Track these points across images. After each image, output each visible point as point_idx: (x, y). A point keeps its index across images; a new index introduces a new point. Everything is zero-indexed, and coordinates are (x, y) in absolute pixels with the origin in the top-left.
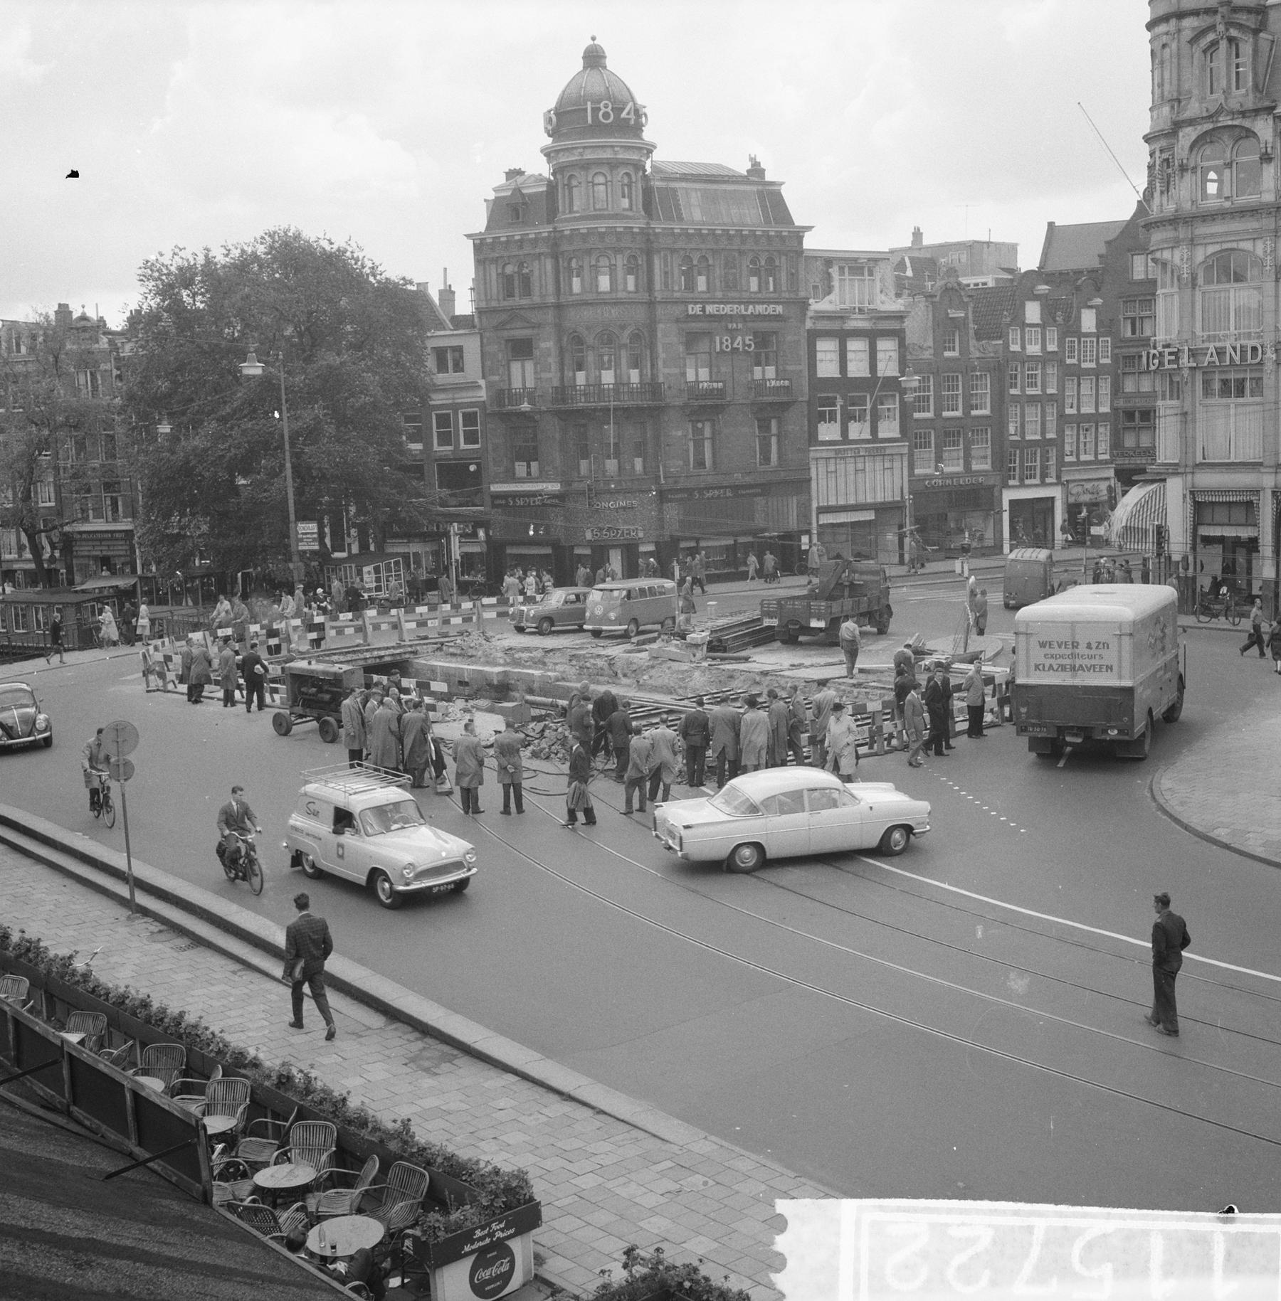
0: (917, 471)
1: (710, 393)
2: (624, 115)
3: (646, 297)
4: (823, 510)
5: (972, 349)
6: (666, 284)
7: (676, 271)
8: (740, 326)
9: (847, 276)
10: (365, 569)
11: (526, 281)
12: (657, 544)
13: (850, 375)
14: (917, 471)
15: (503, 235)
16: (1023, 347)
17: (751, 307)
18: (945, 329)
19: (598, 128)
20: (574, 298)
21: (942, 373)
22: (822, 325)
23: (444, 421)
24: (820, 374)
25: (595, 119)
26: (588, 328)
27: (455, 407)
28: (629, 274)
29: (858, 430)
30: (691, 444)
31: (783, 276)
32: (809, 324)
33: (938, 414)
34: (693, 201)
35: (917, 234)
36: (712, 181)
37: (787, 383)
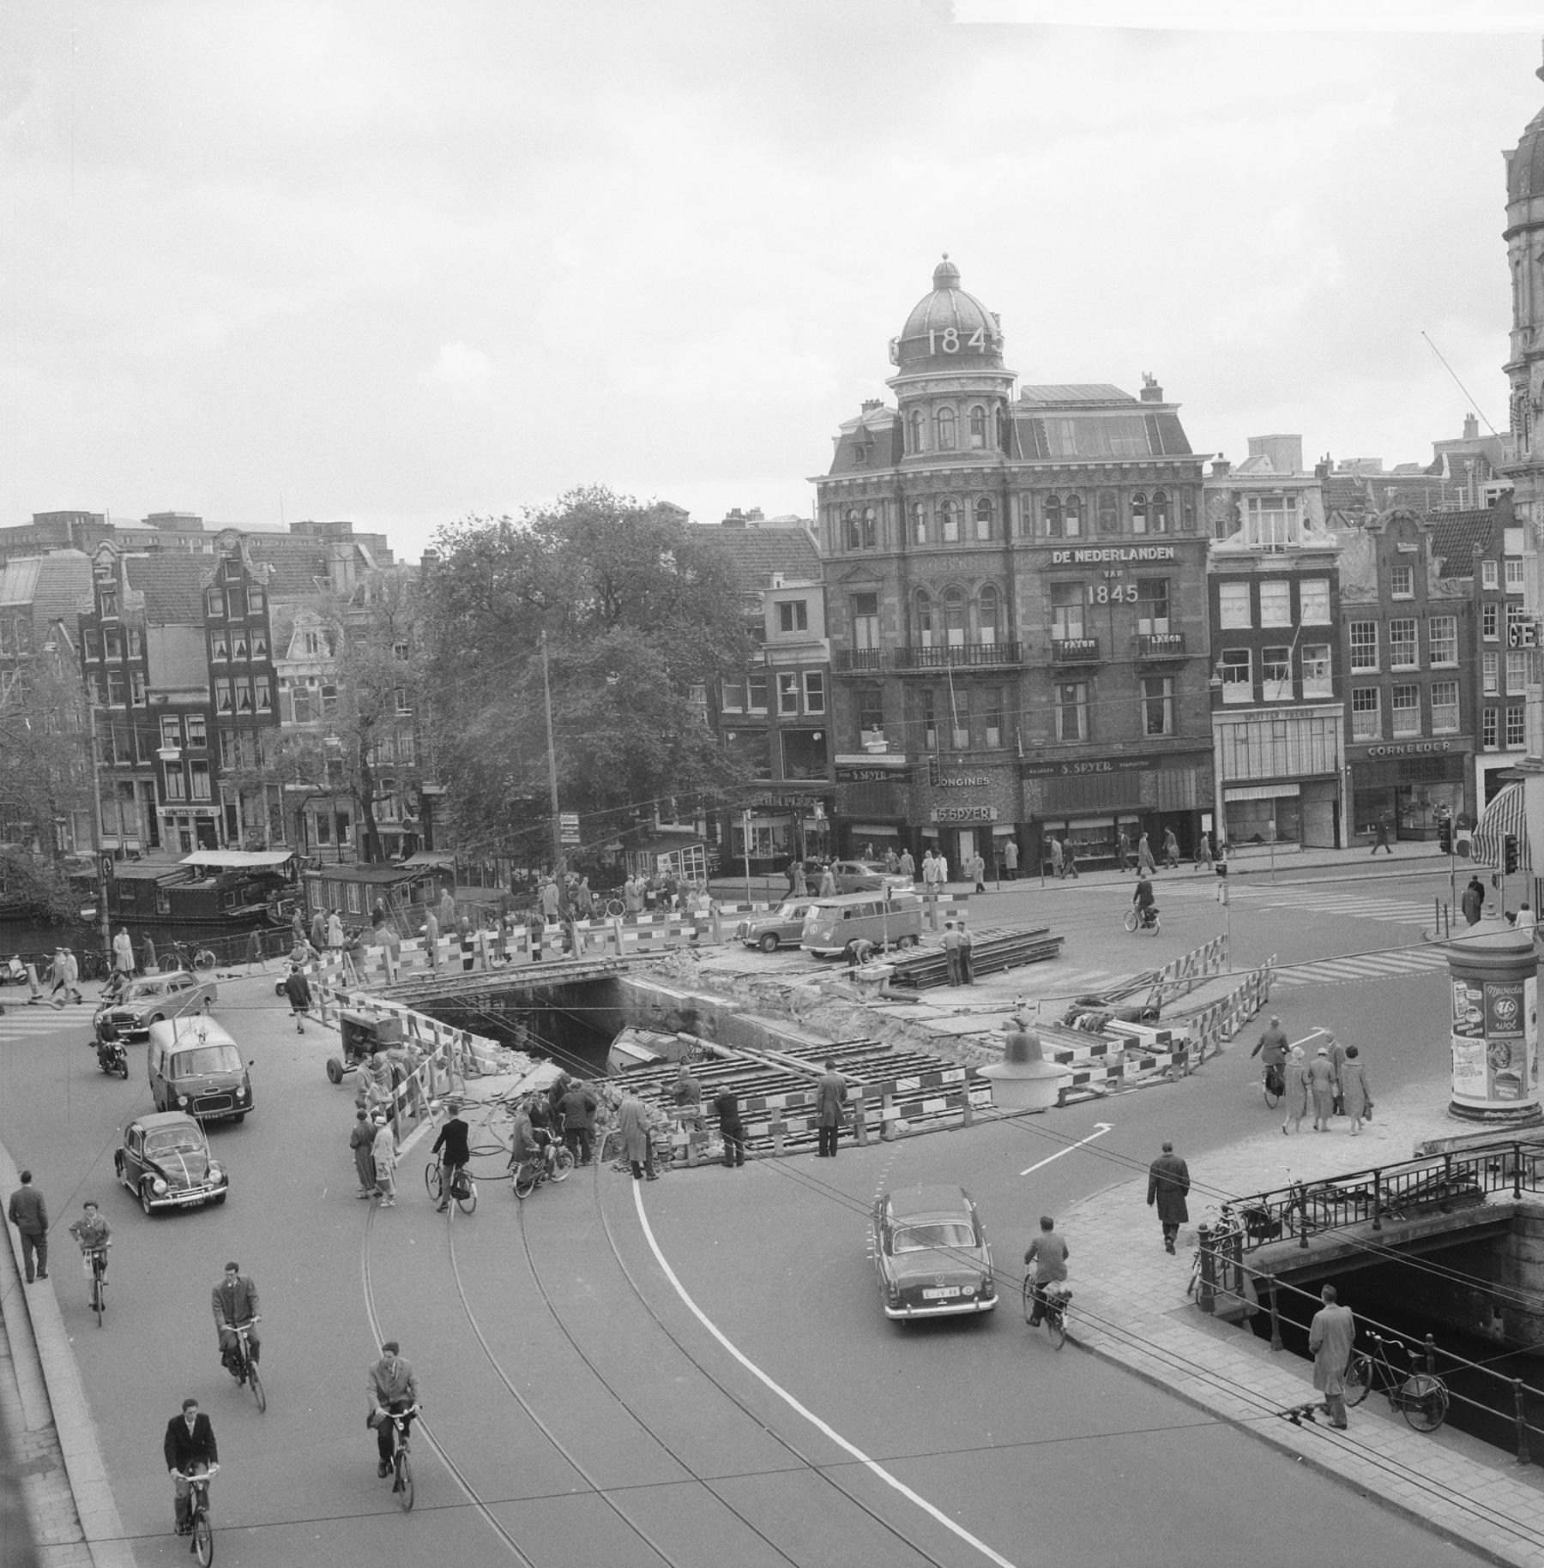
2: (972, 342)
3: (1002, 544)
4: (1227, 785)
5: (1431, 589)
6: (1026, 529)
8: (1120, 573)
9: (1259, 510)
10: (660, 858)
11: (870, 529)
12: (1016, 826)
13: (1264, 625)
14: (1357, 737)
15: (845, 479)
16: (1502, 583)
18: (1394, 566)
19: (943, 359)
20: (920, 548)
21: (1397, 620)
22: (1225, 569)
25: (946, 347)
26: (932, 582)
27: (799, 668)
29: (1274, 690)
32: (1210, 568)
33: (1385, 666)
34: (1065, 433)
35: (1471, 423)
36: (1089, 406)
37: (1178, 638)
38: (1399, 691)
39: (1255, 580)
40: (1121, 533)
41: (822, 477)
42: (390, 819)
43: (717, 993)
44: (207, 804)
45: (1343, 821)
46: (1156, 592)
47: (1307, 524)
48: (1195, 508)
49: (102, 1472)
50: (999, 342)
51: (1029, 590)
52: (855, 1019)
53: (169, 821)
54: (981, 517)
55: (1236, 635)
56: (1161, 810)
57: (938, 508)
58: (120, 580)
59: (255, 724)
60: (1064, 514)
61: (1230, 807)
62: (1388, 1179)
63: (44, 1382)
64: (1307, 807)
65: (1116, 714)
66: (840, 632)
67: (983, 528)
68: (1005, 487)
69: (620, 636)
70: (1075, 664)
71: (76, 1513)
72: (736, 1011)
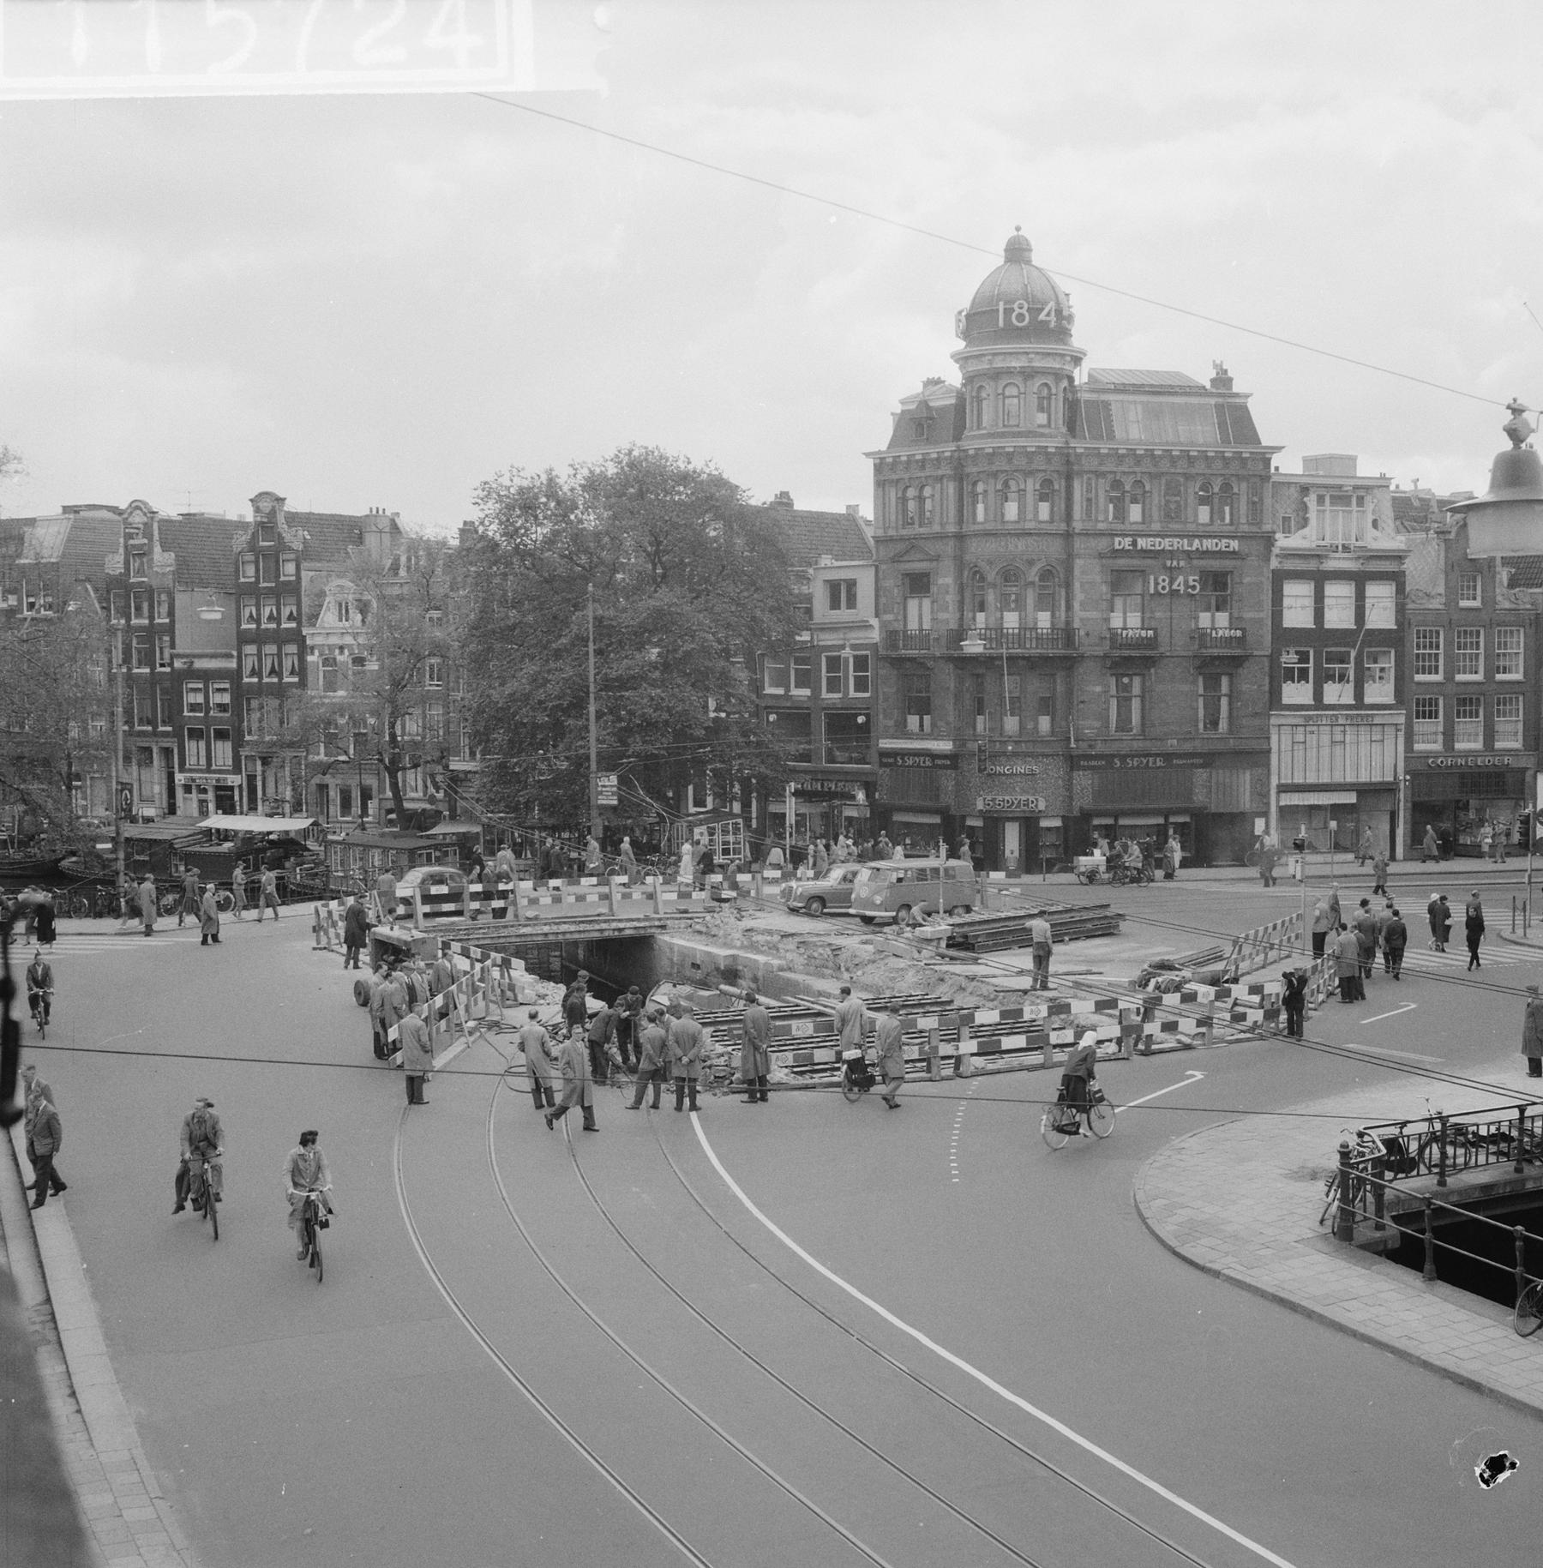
0: (1417, 747)
1: (1141, 643)
2: (1042, 317)
3: (1063, 526)
4: (1284, 789)
5: (1499, 598)
6: (1088, 513)
7: (1102, 500)
8: (1182, 563)
14: (1417, 747)
17: (1197, 541)
19: (1012, 332)
20: (976, 527)
21: (1463, 627)
22: (1290, 565)
23: (834, 664)
24: (1287, 623)
25: (1016, 323)
26: (990, 563)
28: (1041, 500)
29: (1336, 693)
30: (1114, 702)
31: (1243, 507)
32: (1274, 563)
33: (1449, 677)
34: (1132, 416)
36: (1159, 392)
37: (1239, 633)
38: (1462, 702)
39: (1320, 579)
40: (1185, 523)
41: (880, 452)
42: (416, 791)
43: (762, 953)
44: (227, 772)
45: (1400, 831)
46: (1218, 586)
47: (1375, 524)
48: (1261, 499)
49: (102, 1348)
50: (1070, 318)
51: (1088, 574)
52: (911, 977)
53: (188, 789)
54: (1043, 498)
55: (1298, 636)
56: (1213, 809)
57: (999, 487)
58: (151, 539)
59: (280, 691)
60: (1127, 500)
61: (1285, 812)
62: (1533, 1118)
63: (40, 1262)
64: (1364, 817)
65: (1178, 701)
66: (891, 612)
67: (1044, 509)
68: (1069, 467)
69: (665, 597)
70: (1134, 653)
71: (71, 1386)
72: (781, 969)
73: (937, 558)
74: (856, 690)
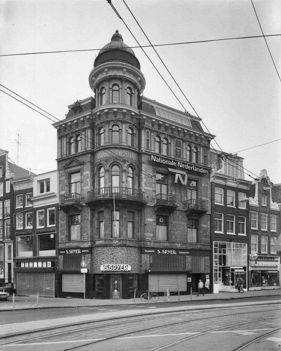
15: (74, 119)
22: (218, 181)
26: (106, 161)
73: (83, 164)
74: (50, 224)
